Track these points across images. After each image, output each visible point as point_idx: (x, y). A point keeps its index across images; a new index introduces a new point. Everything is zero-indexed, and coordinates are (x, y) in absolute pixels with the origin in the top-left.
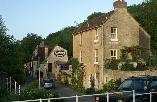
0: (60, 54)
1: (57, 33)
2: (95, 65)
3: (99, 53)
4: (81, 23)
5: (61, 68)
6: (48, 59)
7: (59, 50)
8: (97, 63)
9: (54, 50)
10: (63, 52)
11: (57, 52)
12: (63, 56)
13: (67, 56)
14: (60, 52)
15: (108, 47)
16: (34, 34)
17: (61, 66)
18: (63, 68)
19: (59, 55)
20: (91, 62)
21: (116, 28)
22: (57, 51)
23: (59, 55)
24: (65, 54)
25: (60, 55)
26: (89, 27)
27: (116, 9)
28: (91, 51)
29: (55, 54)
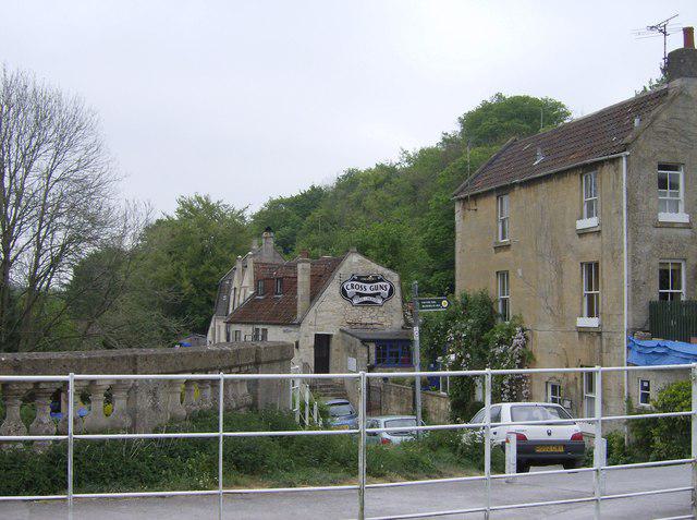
0: (369, 291)
1: (304, 195)
2: (582, 331)
3: (605, 282)
4: (422, 151)
5: (377, 355)
6: (311, 317)
7: (361, 273)
8: (593, 322)
9: (340, 271)
10: (381, 280)
11: (355, 283)
12: (380, 301)
13: (399, 301)
14: (364, 282)
15: (646, 248)
16: (213, 201)
17: (378, 349)
18: (384, 354)
19: (362, 295)
20: (561, 319)
21: (675, 167)
22: (354, 280)
23: (362, 295)
24: (391, 292)
25: (365, 299)
26: (541, 166)
27: (677, 83)
28: (560, 273)
29: (344, 292)
